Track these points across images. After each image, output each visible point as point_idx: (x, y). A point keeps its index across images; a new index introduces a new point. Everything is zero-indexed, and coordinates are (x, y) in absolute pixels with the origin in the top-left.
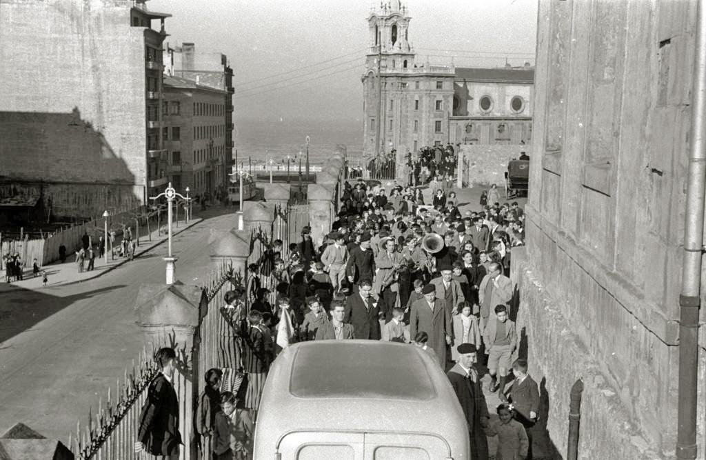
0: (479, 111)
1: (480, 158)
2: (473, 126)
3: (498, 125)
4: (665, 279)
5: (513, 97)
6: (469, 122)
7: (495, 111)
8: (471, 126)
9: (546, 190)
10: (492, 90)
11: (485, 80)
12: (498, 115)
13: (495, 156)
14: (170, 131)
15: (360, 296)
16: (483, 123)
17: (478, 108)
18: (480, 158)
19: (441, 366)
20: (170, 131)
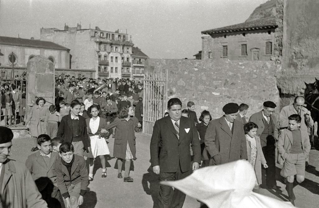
0: (9, 63)
1: (181, 82)
2: (6, 72)
3: (78, 74)
4: (246, 49)
5: (30, 55)
6: (4, 70)
7: (19, 63)
8: (5, 72)
9: (155, 111)
10: (17, 50)
11: (11, 44)
12: (21, 66)
13: (204, 78)
14: (114, 69)
15: (192, 166)
16: (87, 74)
17: (8, 62)
18: (181, 82)
19: (282, 201)
20: (114, 69)
